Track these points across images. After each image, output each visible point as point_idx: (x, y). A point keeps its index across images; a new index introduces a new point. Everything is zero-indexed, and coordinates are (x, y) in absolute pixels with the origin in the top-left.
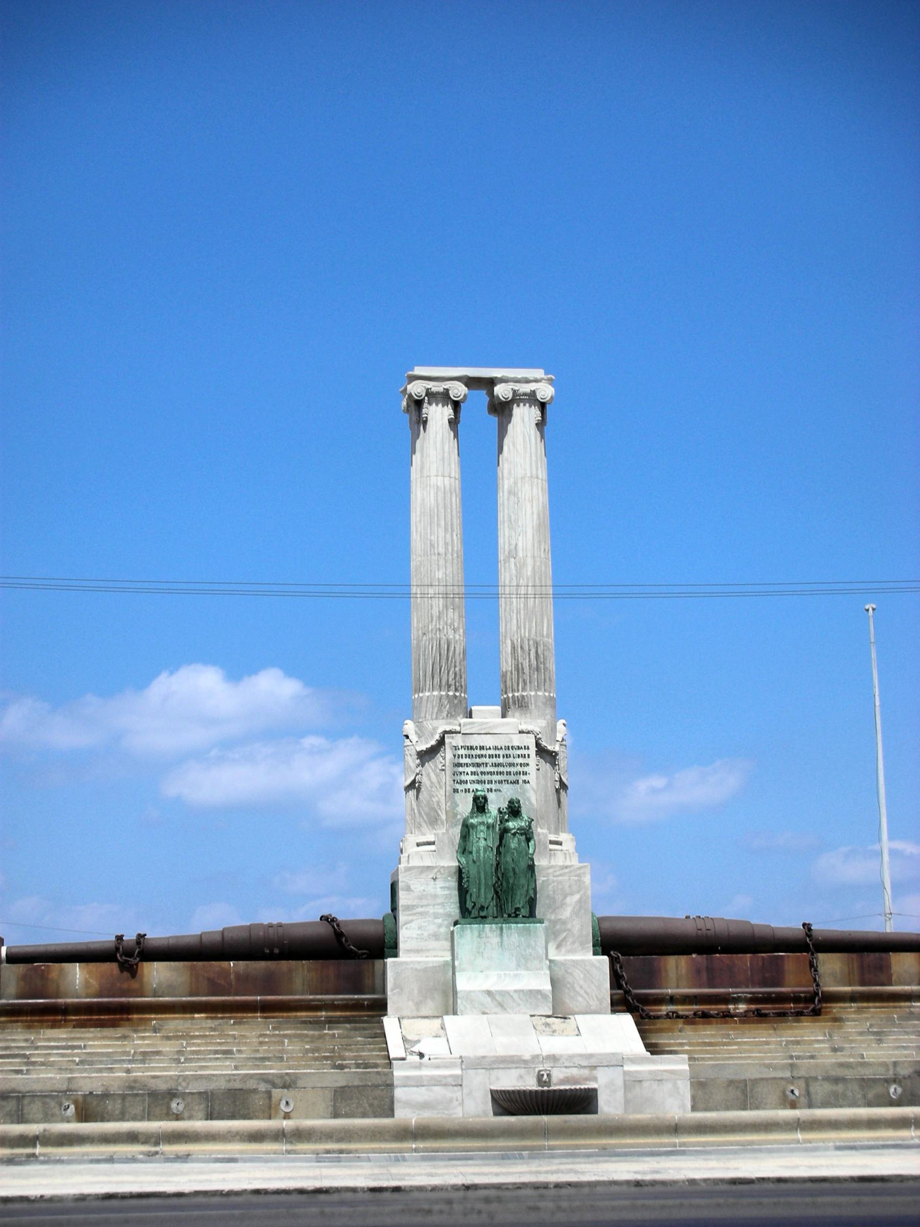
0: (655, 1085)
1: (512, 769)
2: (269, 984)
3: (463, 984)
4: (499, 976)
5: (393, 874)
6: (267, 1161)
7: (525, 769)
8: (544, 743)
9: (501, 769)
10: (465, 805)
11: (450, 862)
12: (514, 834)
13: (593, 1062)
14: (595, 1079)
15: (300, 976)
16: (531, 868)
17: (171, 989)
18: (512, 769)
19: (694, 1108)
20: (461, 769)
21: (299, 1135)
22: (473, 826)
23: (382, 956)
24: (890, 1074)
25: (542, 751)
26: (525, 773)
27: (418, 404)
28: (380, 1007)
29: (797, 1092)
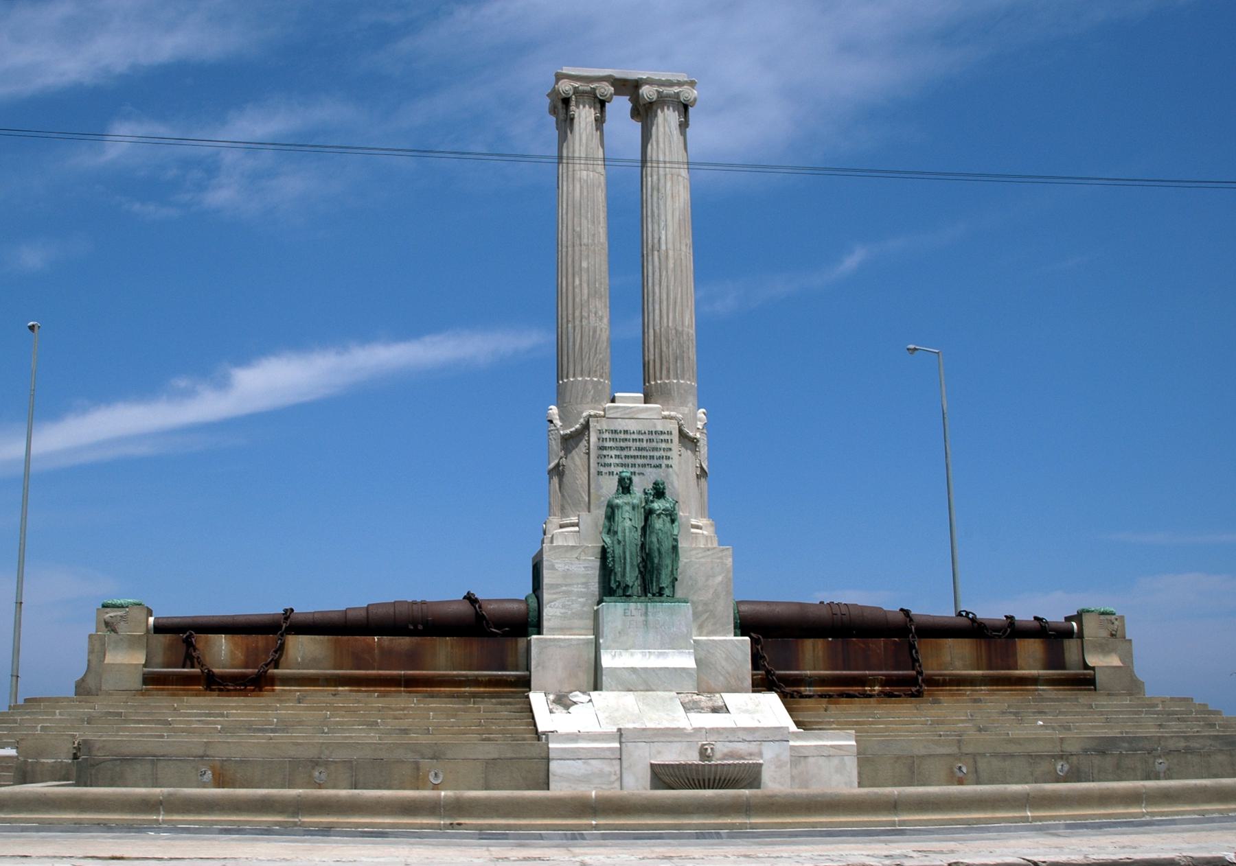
0: (821, 761)
2: (412, 659)
3: (607, 661)
5: (536, 556)
6: (421, 836)
7: (669, 454)
8: (686, 430)
9: (644, 453)
10: (609, 486)
11: (594, 545)
12: (659, 515)
13: (758, 736)
14: (760, 755)
15: (444, 655)
16: (675, 548)
17: (314, 662)
18: (656, 454)
19: (860, 785)
20: (605, 452)
21: (459, 808)
22: (618, 506)
23: (526, 634)
24: (1057, 751)
25: (683, 435)
26: (668, 458)
27: (566, 101)
28: (525, 683)
29: (964, 770)
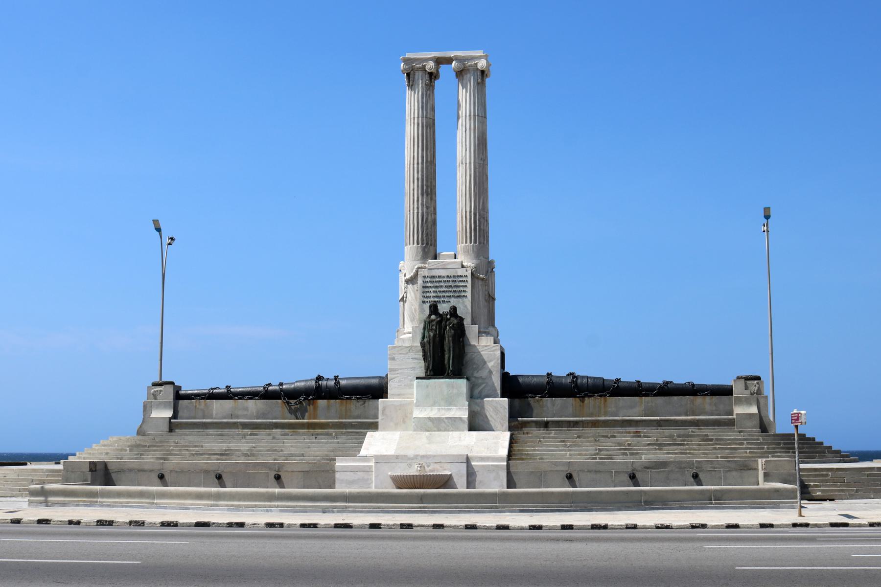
1: (457, 289)
4: (439, 410)
18: (457, 289)
26: (465, 291)
